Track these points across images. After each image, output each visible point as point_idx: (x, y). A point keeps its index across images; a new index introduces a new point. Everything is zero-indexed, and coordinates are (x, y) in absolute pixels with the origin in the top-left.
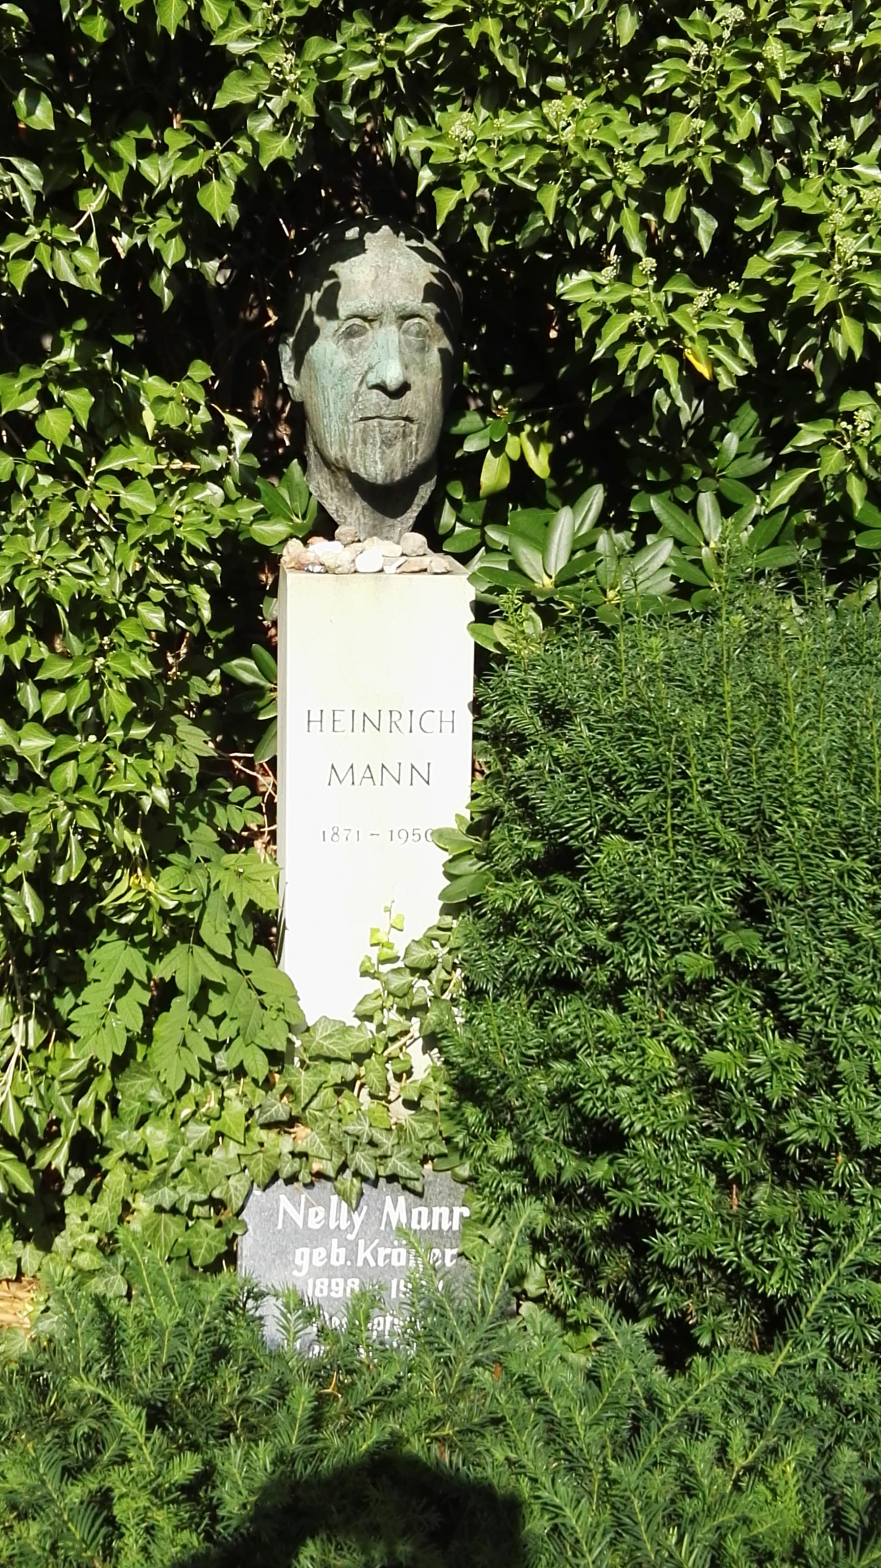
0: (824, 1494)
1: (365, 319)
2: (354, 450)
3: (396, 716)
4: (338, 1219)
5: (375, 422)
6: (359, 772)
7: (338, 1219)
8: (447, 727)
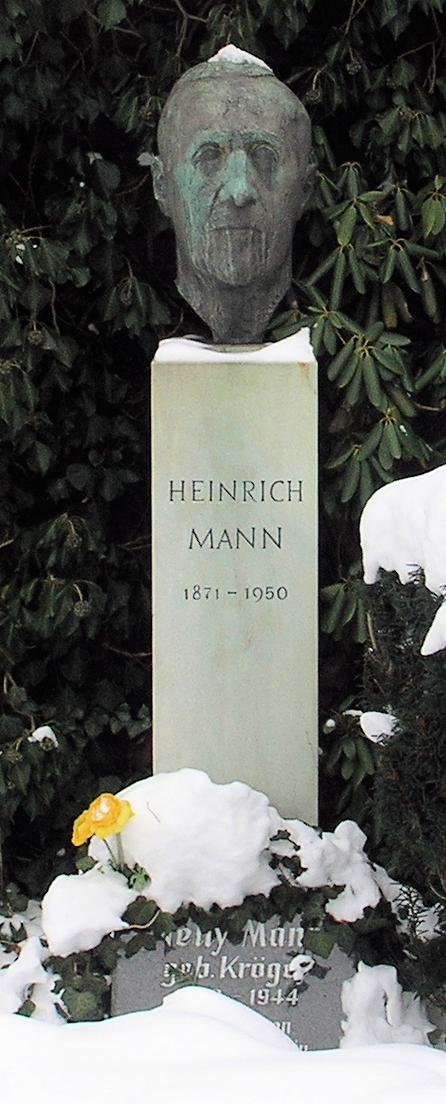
3: (249, 486)
8: (295, 496)
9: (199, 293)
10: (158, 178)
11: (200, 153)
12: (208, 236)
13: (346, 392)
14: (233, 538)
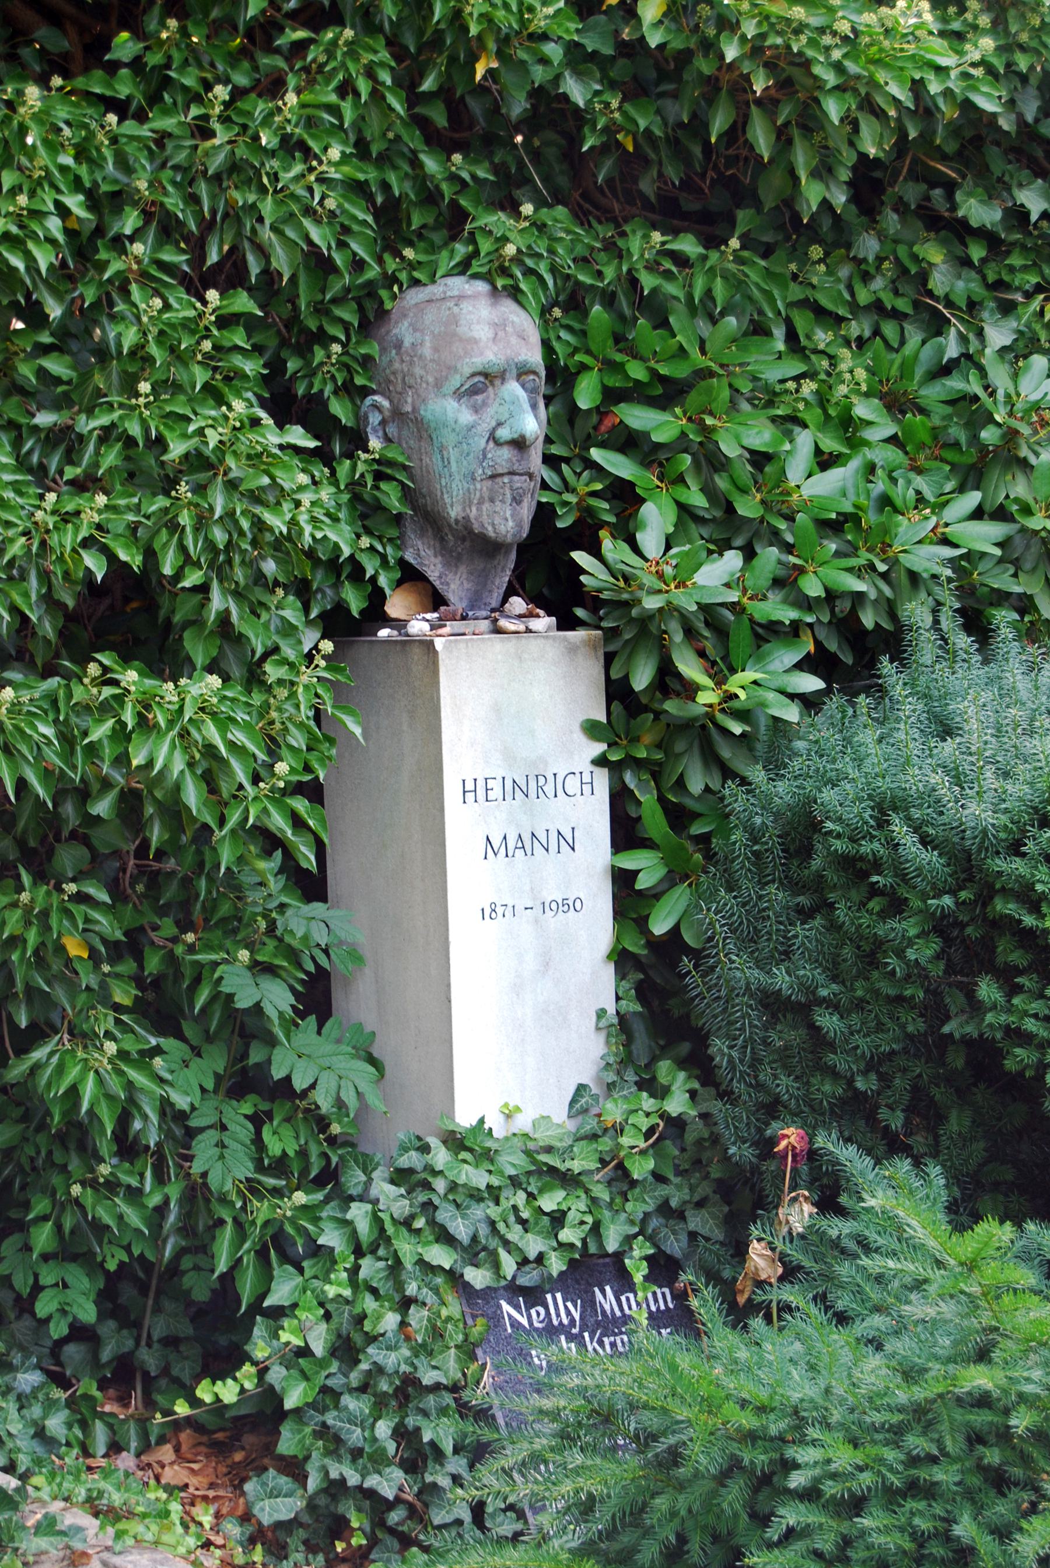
0: (267, 1412)
1: (486, 375)
3: (542, 780)
4: (558, 1315)
5: (506, 480)
6: (512, 843)
7: (558, 1315)
8: (587, 789)
13: (233, 1279)
14: (527, 843)
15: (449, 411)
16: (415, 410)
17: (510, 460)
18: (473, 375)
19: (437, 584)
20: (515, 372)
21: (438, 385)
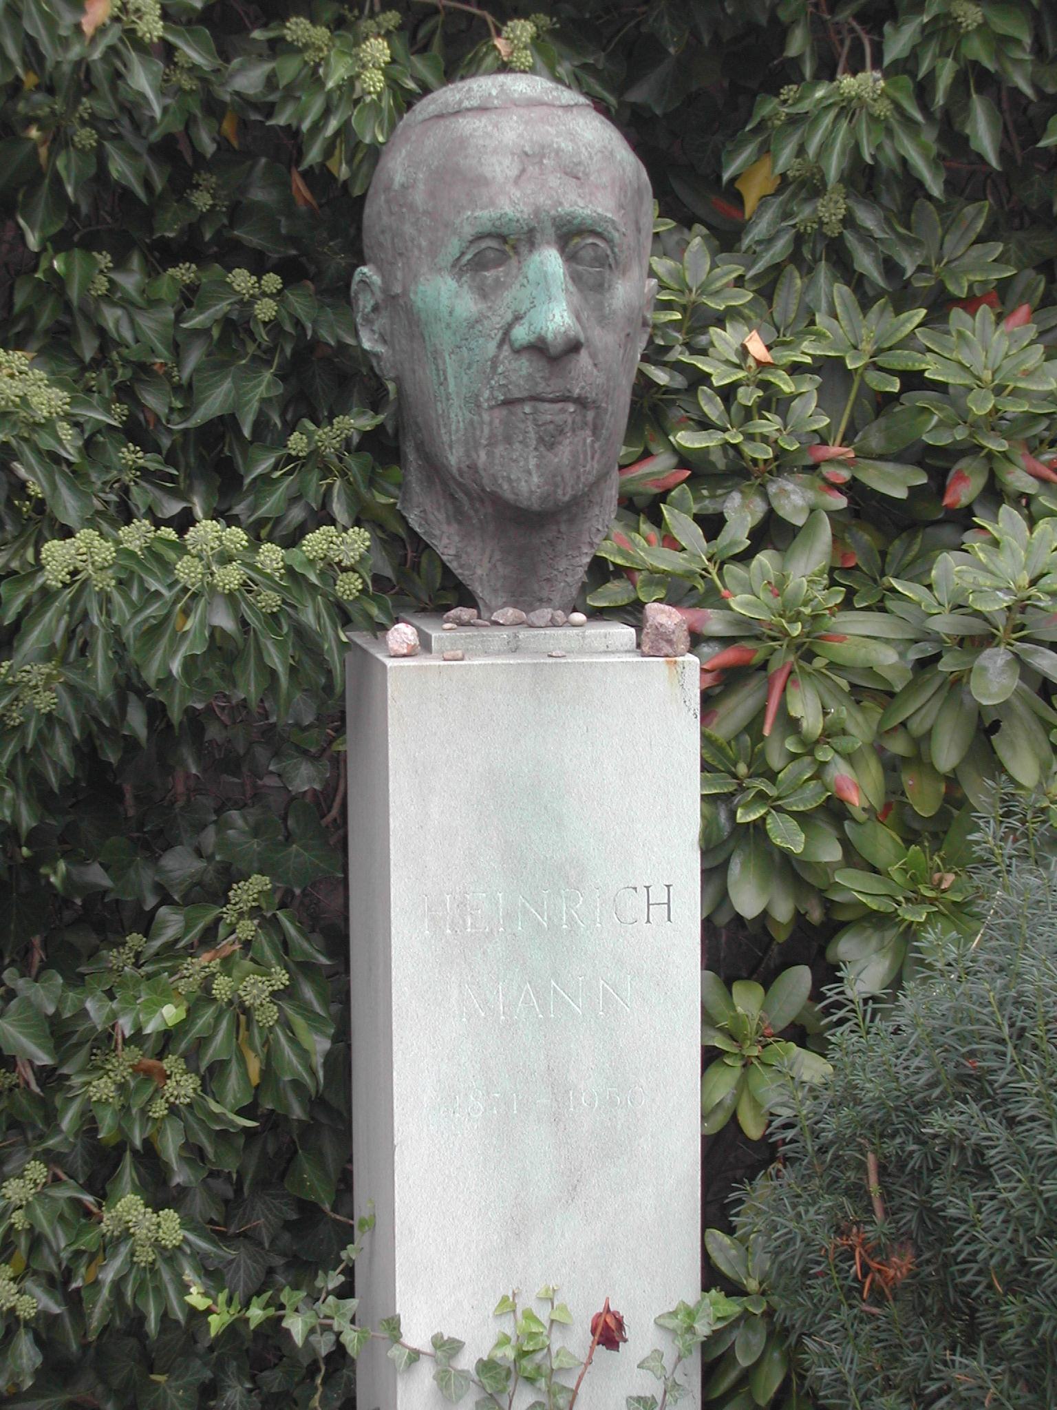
1: (503, 238)
2: (490, 455)
8: (658, 912)
9: (454, 528)
10: (368, 309)
11: (468, 257)
12: (486, 417)
15: (444, 295)
16: (405, 292)
17: (530, 377)
18: (480, 237)
19: (453, 566)
20: (551, 232)
21: (434, 250)
